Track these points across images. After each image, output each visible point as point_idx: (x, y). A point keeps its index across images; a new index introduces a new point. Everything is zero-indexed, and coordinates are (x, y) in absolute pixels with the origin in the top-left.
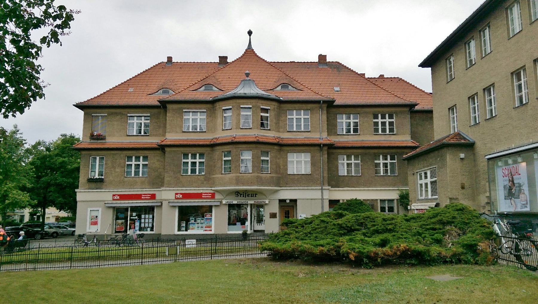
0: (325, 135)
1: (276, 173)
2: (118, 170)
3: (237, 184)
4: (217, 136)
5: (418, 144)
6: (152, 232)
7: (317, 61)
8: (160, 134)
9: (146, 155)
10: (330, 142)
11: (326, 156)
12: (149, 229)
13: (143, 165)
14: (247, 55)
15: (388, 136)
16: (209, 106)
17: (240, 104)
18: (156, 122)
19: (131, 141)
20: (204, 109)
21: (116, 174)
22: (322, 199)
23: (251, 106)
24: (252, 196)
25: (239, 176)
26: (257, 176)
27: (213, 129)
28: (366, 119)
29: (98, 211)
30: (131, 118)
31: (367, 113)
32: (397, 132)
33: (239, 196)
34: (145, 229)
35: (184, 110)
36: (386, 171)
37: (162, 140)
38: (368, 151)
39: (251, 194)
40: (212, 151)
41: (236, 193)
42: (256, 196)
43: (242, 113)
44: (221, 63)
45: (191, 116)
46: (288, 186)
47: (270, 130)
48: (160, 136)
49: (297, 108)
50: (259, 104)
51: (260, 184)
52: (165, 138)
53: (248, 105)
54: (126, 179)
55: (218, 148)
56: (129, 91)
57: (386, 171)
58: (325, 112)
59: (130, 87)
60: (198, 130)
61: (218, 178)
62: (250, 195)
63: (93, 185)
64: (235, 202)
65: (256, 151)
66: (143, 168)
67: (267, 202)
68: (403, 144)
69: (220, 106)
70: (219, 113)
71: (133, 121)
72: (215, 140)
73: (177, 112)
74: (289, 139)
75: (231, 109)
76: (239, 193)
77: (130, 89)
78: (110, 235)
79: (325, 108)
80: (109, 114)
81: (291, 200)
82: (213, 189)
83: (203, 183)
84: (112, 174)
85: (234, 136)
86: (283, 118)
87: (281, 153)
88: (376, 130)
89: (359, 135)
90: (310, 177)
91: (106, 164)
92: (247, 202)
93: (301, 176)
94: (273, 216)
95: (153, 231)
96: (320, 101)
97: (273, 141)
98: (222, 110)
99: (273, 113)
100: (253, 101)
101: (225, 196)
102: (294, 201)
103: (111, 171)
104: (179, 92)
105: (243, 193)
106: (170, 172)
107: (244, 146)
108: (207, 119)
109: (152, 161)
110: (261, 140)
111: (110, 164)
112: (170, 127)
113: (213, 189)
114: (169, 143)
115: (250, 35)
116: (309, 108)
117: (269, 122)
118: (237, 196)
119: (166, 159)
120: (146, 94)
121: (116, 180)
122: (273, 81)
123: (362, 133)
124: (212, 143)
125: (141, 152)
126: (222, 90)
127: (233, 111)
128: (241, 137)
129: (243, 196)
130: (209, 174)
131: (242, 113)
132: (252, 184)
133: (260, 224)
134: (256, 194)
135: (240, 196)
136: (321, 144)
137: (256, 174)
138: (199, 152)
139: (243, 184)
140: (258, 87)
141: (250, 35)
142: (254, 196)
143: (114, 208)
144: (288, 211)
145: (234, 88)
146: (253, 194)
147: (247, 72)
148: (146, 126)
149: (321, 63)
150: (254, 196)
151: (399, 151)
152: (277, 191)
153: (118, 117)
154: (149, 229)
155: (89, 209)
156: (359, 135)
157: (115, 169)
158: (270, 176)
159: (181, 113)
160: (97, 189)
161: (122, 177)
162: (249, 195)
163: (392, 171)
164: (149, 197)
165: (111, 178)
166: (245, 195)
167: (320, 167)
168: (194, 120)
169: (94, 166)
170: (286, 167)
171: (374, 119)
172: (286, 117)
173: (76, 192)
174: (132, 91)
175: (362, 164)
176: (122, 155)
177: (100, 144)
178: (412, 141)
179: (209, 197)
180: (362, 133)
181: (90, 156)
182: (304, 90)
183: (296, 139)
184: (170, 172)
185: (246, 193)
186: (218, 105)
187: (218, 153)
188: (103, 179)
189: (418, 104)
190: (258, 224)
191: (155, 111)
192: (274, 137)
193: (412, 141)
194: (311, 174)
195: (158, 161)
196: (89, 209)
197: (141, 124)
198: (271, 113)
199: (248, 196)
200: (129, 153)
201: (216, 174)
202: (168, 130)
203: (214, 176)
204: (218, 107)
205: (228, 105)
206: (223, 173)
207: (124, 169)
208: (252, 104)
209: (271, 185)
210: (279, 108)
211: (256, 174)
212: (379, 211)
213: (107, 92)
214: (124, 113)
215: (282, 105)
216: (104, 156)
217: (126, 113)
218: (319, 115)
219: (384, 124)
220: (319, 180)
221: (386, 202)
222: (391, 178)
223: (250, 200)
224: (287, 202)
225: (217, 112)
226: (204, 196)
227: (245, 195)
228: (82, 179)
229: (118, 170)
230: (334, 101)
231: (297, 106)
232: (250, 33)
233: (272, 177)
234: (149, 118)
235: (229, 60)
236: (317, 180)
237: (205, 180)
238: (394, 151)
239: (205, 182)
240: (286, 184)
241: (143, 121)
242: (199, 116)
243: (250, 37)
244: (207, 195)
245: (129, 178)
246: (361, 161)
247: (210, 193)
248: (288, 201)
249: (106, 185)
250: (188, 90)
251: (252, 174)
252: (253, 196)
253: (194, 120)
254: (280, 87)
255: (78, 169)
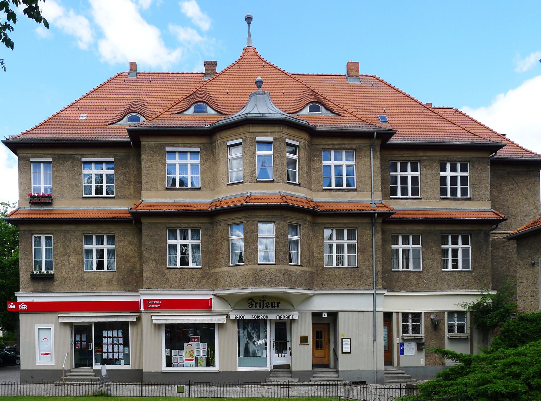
0: (378, 197)
1: (309, 264)
2: (72, 259)
3: (254, 284)
4: (220, 196)
5: (503, 216)
6: (127, 367)
7: (344, 73)
8: (131, 195)
9: (112, 233)
10: (387, 209)
11: (380, 235)
12: (123, 362)
13: (108, 250)
14: (245, 60)
15: (460, 201)
16: (204, 140)
17: (256, 134)
18: (124, 174)
19: (89, 208)
20: (197, 146)
21: (72, 266)
22: (374, 311)
23: (271, 139)
24: (272, 307)
25: (256, 270)
26: (284, 270)
27: (212, 185)
28: (430, 171)
29: (48, 331)
30: (86, 166)
31: (431, 160)
32: (473, 193)
33: (254, 305)
34: (117, 362)
35: (167, 149)
36: (455, 266)
37: (137, 204)
38: (432, 227)
39: (272, 303)
40: (212, 223)
41: (250, 301)
42: (278, 307)
43: (259, 153)
44: (208, 74)
45: (177, 161)
46: (324, 288)
47: (299, 185)
48: (130, 199)
49: (336, 147)
50: (283, 135)
51: (288, 283)
52: (141, 201)
53: (268, 136)
54: (86, 276)
55: (221, 218)
56: (81, 118)
57: (455, 266)
58: (378, 154)
59: (81, 112)
60: (189, 186)
61: (223, 273)
62: (270, 305)
63: (40, 286)
64: (249, 317)
65: (282, 223)
66: (108, 257)
67: (296, 317)
68: (479, 216)
69: (223, 140)
70: (221, 153)
71: (90, 172)
72: (218, 204)
73: (156, 152)
74: (326, 204)
75: (240, 144)
76: (254, 301)
77: (81, 115)
78: (68, 370)
79: (378, 148)
80: (54, 160)
81: (330, 314)
82: (215, 292)
83: (199, 283)
84: (64, 265)
85: (249, 194)
86: (316, 165)
87: (315, 228)
88: (443, 192)
89: (420, 199)
90: (356, 272)
91: (55, 248)
92: (267, 316)
93: (343, 270)
94: (304, 340)
95: (129, 364)
96: (374, 133)
97: (306, 205)
98: (226, 147)
99: (303, 154)
100: (276, 129)
101: (233, 307)
102: (334, 315)
103: (63, 260)
104: (158, 117)
105: (260, 300)
106: (151, 262)
107: (263, 214)
108: (202, 165)
109: (121, 244)
110: (290, 203)
111: (61, 249)
112: (147, 180)
113: (215, 292)
114: (147, 209)
115: (249, 24)
116: (354, 147)
117: (297, 171)
118: (251, 306)
119: (144, 238)
120: (106, 124)
121: (71, 277)
122: (294, 99)
123: (424, 195)
124: (213, 208)
125: (104, 227)
126: (222, 114)
127: (244, 148)
128: (259, 197)
129: (260, 307)
130: (209, 265)
131: (259, 153)
132: (277, 284)
133: (283, 354)
134: (279, 303)
135: (256, 307)
136: (375, 213)
137: (282, 267)
138: (191, 225)
139: (264, 286)
140: (276, 106)
141: (249, 24)
142: (276, 305)
143: (70, 324)
144: (321, 332)
145: (238, 110)
146: (274, 303)
147: (259, 78)
148: (110, 179)
149: (352, 76)
150: (276, 305)
151: (475, 228)
152: (309, 297)
153: (69, 163)
154: (123, 362)
155: (37, 327)
156: (420, 199)
157: (69, 257)
158: (301, 271)
159: (161, 152)
160: (45, 291)
161: (80, 272)
162: (269, 304)
163: (466, 264)
164: (158, 304)
165: (64, 273)
166: (262, 306)
167: (371, 254)
168: (183, 168)
169: (38, 253)
170: (322, 255)
171: (441, 171)
172: (321, 162)
173: (17, 297)
174: (85, 118)
175: (424, 250)
176: (77, 233)
177: (45, 212)
178: (493, 210)
179: (158, 306)
180: (424, 195)
181: (33, 234)
182: (343, 115)
183: (336, 204)
184: (151, 262)
185: (263, 301)
186: (219, 138)
187: (221, 228)
188: (53, 274)
189: (505, 145)
190: (280, 354)
191: (121, 152)
192: (306, 198)
193: (493, 210)
194: (358, 267)
195: (130, 242)
196: (37, 327)
197: (101, 176)
198: (301, 154)
199: (267, 307)
200: (88, 229)
201: (220, 266)
202: (144, 186)
203: (217, 270)
204: (219, 141)
205: (236, 137)
206: (231, 264)
207: (80, 257)
208: (274, 135)
209: (303, 286)
210: (311, 144)
211: (282, 267)
212: (456, 332)
213: (50, 121)
214: (76, 156)
215: (316, 141)
216: (52, 234)
217: (79, 157)
218: (369, 160)
219: (454, 180)
220: (369, 278)
221: (456, 316)
222: (463, 275)
223: (271, 312)
224: (324, 316)
225: (217, 151)
226: (150, 304)
227: (262, 306)
228: (24, 277)
229: (72, 259)
230: (391, 134)
231: (337, 142)
232: (249, 19)
233: (304, 272)
234: (113, 166)
235: (218, 70)
236: (367, 278)
237: (203, 277)
238: (467, 228)
239: (203, 282)
240: (323, 285)
241: (105, 172)
242: (189, 161)
243: (249, 26)
244: (155, 302)
245: (90, 274)
246: (422, 246)
247: (158, 300)
248: (325, 316)
249: (58, 286)
250: (170, 113)
251: (277, 267)
252: (275, 307)
253: (183, 168)
254: (307, 109)
255: (16, 262)
